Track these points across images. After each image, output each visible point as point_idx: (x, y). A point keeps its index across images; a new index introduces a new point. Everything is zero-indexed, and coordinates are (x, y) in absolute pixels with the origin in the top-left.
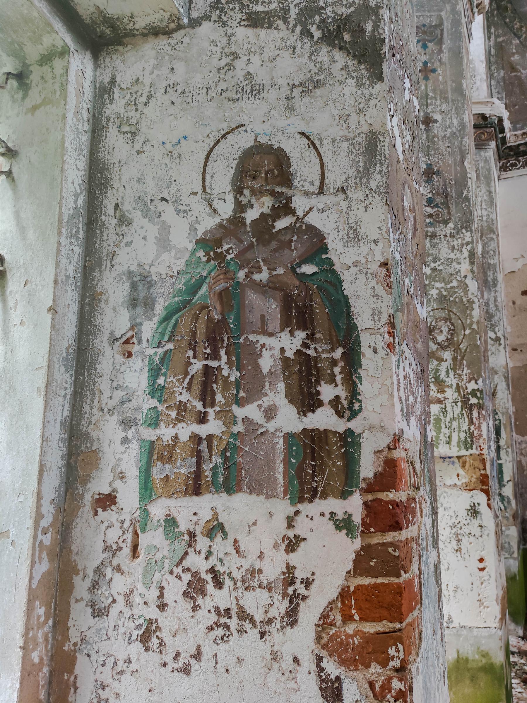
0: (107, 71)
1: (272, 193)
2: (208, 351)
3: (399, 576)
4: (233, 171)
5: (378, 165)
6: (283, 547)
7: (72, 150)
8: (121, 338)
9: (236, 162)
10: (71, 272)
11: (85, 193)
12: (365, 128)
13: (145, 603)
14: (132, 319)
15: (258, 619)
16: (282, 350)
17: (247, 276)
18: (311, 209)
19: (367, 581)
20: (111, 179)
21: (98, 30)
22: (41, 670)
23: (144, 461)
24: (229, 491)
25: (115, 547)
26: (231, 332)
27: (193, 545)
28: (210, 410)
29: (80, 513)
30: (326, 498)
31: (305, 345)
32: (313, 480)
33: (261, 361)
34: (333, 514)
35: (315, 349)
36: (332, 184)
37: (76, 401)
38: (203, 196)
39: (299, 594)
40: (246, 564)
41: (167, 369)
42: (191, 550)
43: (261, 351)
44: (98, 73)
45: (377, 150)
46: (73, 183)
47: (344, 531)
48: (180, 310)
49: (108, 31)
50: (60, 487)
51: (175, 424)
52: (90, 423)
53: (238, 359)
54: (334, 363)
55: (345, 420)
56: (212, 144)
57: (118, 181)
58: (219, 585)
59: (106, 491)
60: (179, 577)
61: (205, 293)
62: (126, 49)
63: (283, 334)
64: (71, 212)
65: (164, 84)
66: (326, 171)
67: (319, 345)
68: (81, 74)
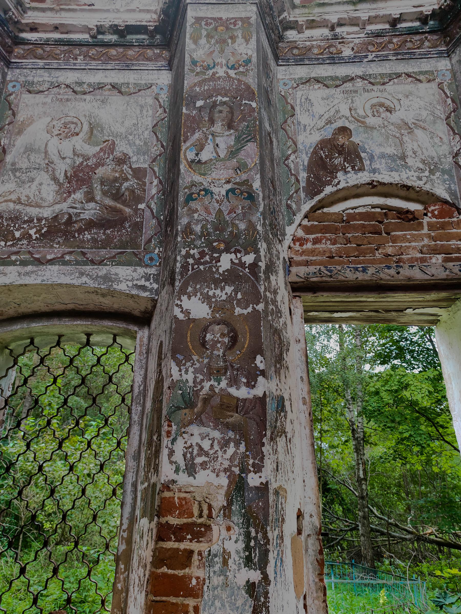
22: (122, 593)
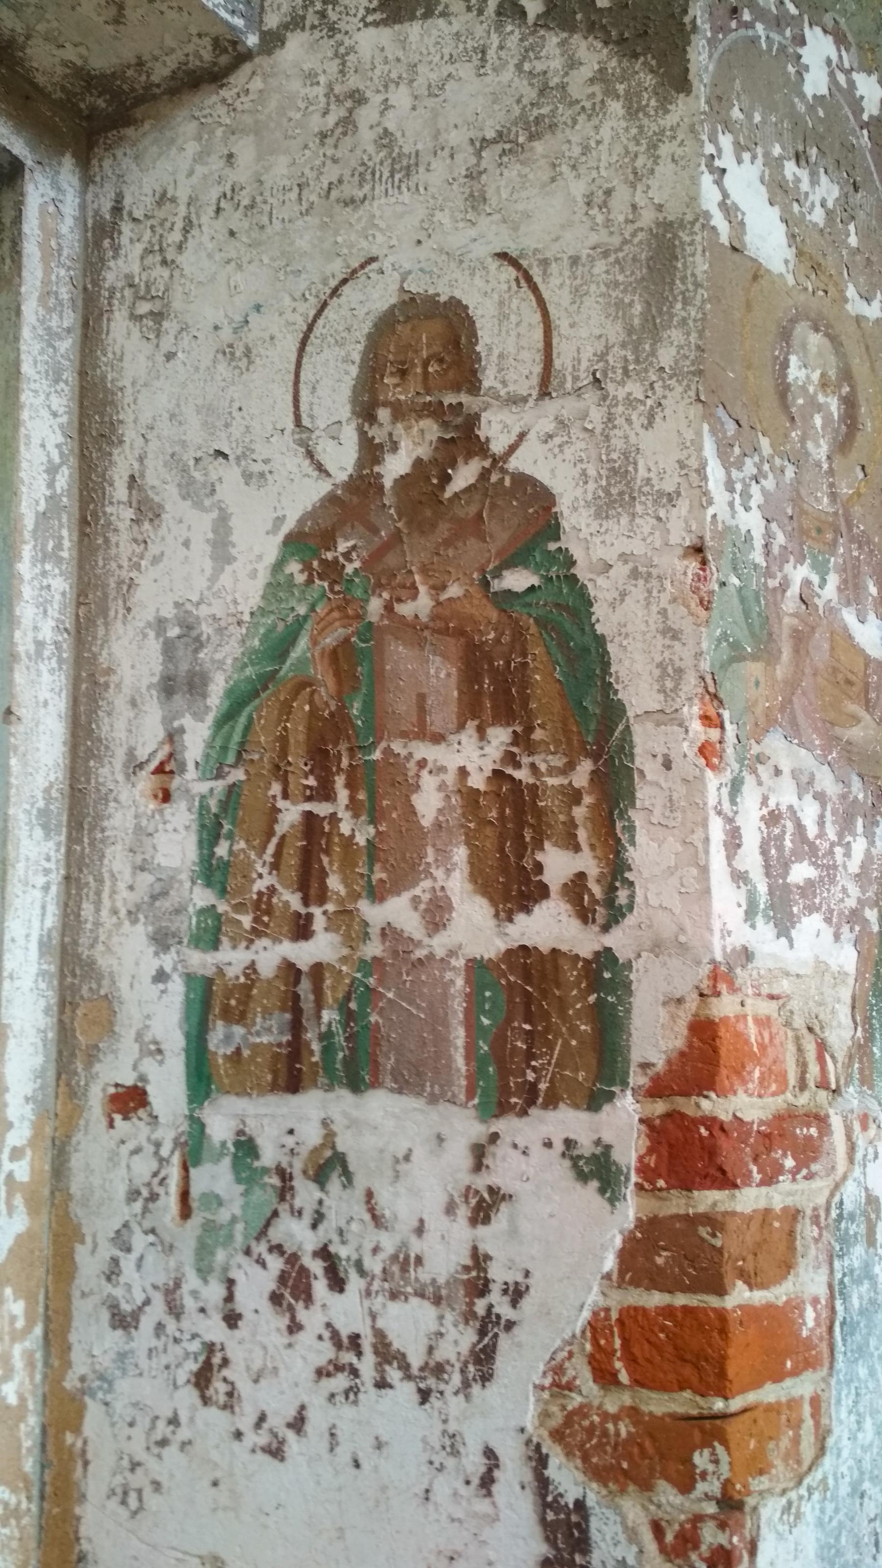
0: (107, 186)
1: (436, 411)
2: (312, 781)
3: (721, 1291)
4: (354, 371)
5: (679, 306)
6: (463, 1212)
7: (37, 377)
8: (148, 761)
9: (360, 347)
10: (47, 632)
11: (73, 461)
12: (648, 217)
13: (202, 1310)
14: (167, 721)
15: (416, 1361)
16: (463, 772)
17: (389, 608)
18: (522, 436)
19: (655, 1299)
20: (121, 422)
21: (82, 106)
22: (22, 1418)
23: (195, 1020)
24: (356, 1086)
25: (145, 1193)
26: (357, 737)
27: (288, 1197)
28: (316, 911)
29: (82, 1122)
30: (555, 1108)
31: (511, 759)
32: (529, 1066)
33: (417, 800)
34: (569, 1143)
35: (533, 767)
36: (570, 369)
37: (68, 894)
38: (297, 437)
39: (498, 1317)
40: (389, 1243)
41: (233, 823)
42: (284, 1208)
43: (418, 776)
44: (89, 196)
45: (675, 268)
46: (43, 446)
47: (595, 1184)
48: (256, 694)
49: (101, 103)
50: (44, 1069)
51: (251, 941)
52: (96, 940)
53: (373, 796)
54: (575, 797)
55: (596, 929)
56: (312, 313)
57: (132, 425)
58: (337, 1283)
59: (129, 1079)
60: (263, 1264)
61: (305, 653)
62: (141, 131)
63: (464, 737)
64: (42, 507)
65: (214, 193)
66: (555, 341)
67: (543, 756)
68: (51, 209)
